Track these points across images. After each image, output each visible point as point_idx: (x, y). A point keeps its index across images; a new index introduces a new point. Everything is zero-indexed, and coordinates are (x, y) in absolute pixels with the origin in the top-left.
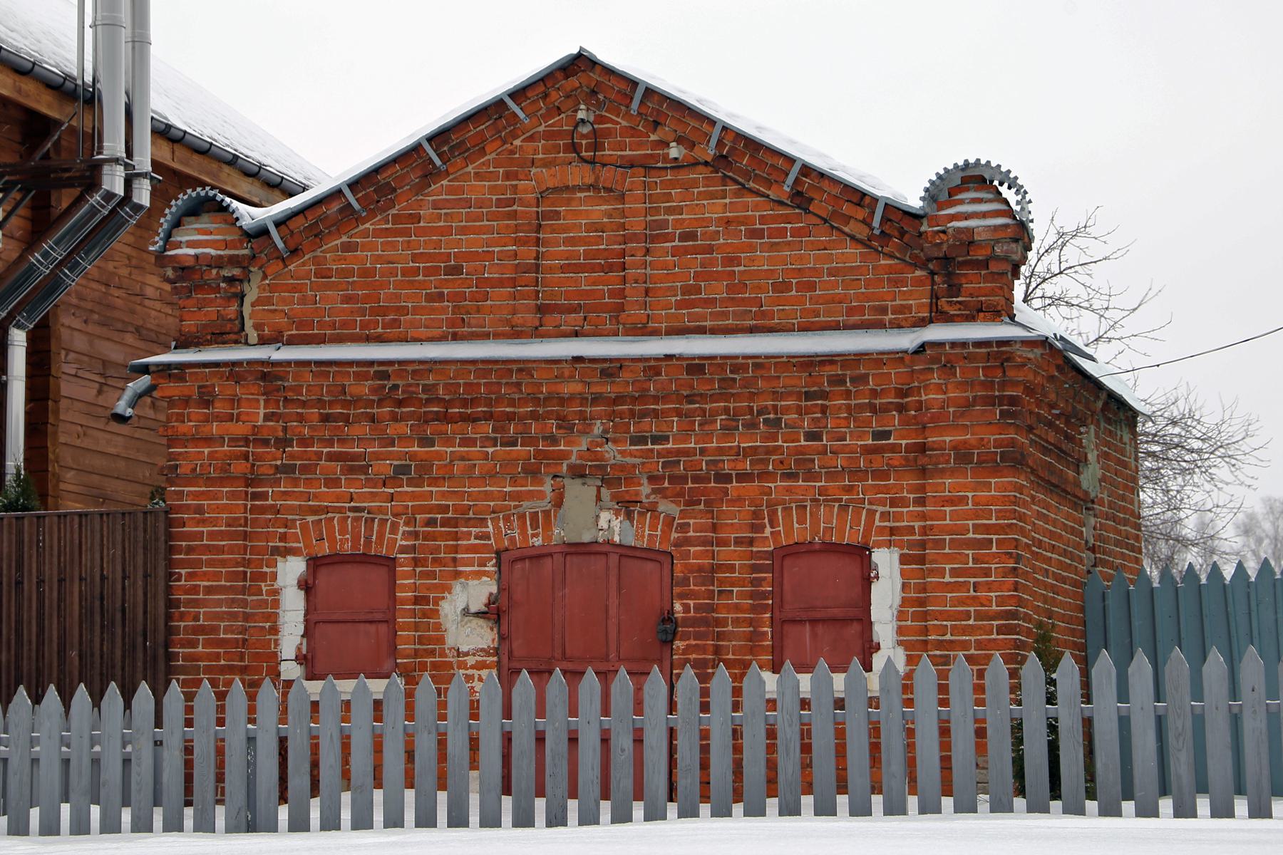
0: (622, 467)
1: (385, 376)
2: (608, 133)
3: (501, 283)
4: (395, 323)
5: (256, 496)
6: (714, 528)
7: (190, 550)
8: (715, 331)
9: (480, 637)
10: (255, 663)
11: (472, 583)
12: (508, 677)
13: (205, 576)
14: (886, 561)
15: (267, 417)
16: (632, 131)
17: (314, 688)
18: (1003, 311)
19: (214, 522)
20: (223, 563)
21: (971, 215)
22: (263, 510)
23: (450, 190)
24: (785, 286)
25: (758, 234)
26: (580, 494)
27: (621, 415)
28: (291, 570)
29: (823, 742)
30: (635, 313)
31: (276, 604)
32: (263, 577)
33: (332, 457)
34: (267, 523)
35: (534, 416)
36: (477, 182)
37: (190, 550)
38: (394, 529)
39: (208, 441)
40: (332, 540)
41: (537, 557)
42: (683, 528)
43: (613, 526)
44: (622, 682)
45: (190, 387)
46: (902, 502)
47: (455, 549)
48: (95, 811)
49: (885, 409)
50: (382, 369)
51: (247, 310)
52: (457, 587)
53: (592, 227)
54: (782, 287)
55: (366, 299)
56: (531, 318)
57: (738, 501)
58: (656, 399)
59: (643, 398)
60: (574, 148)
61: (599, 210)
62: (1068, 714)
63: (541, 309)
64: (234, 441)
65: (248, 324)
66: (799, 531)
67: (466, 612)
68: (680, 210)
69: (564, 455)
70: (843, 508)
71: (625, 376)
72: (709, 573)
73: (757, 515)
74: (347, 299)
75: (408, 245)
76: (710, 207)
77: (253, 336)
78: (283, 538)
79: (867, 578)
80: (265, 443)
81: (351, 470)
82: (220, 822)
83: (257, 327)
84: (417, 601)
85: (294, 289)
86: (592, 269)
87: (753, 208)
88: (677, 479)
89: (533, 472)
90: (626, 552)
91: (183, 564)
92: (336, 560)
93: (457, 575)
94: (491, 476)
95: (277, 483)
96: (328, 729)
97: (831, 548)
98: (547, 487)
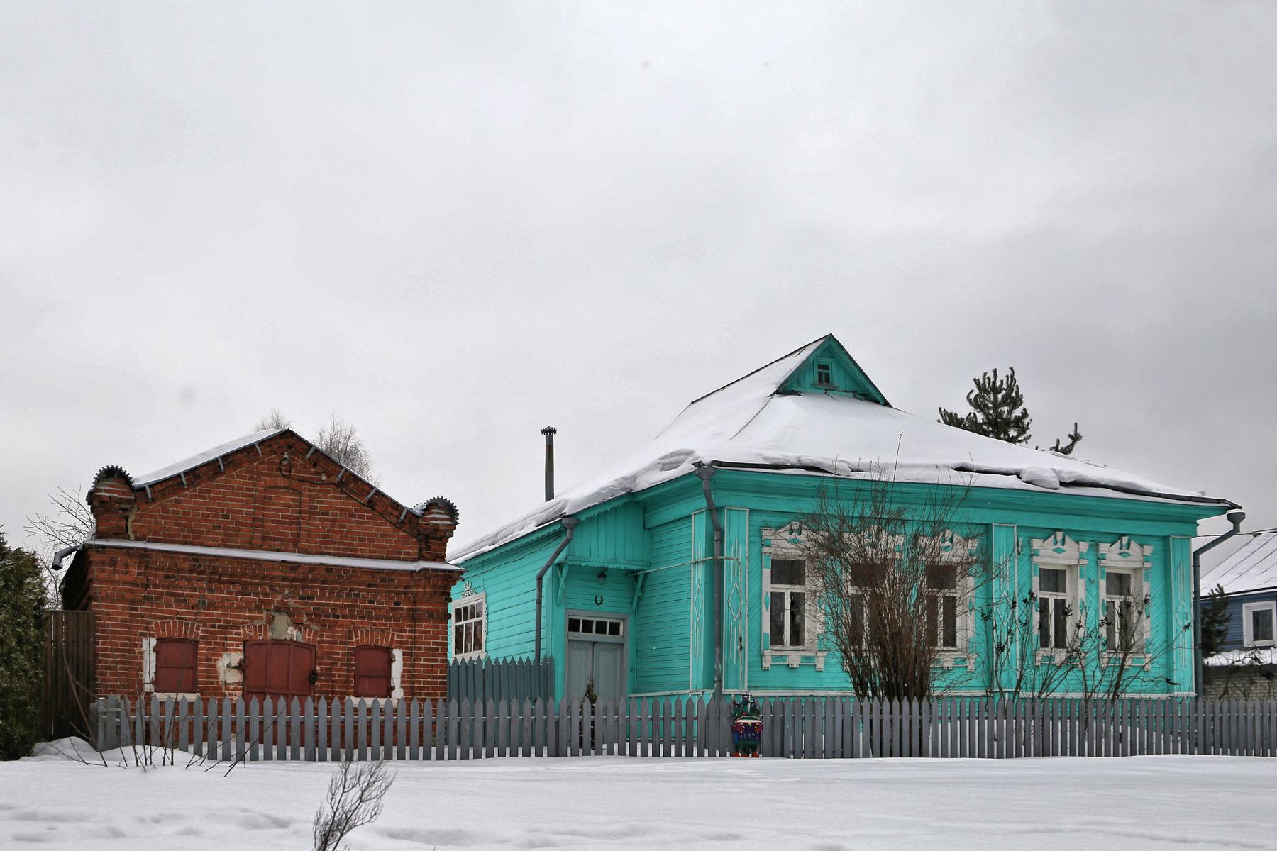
0: (297, 609)
1: (197, 561)
2: (295, 466)
3: (246, 525)
4: (198, 538)
5: (132, 609)
6: (333, 637)
7: (103, 631)
8: (335, 555)
9: (234, 677)
10: (132, 686)
11: (233, 654)
12: (246, 696)
13: (111, 644)
14: (398, 653)
15: (139, 574)
16: (304, 466)
17: (161, 697)
18: (441, 558)
19: (115, 620)
20: (119, 638)
21: (438, 518)
22: (137, 615)
23: (225, 481)
24: (363, 539)
25: (353, 516)
26: (281, 621)
27: (172, 577)
28: (149, 644)
29: (389, 727)
30: (304, 544)
31: (142, 658)
32: (136, 646)
33: (168, 594)
34: (137, 622)
35: (261, 585)
36: (237, 479)
37: (103, 631)
38: (198, 628)
39: (112, 582)
40: (169, 631)
41: (261, 644)
42: (322, 636)
43: (292, 633)
44: (296, 702)
45: (106, 557)
46: (404, 631)
47: (226, 639)
48: (459, 750)
49: (398, 593)
50: (196, 558)
51: (130, 524)
52: (225, 655)
53: (285, 505)
54: (362, 539)
55: (185, 525)
56: (259, 541)
57: (341, 626)
58: (312, 581)
59: (304, 580)
60: (280, 470)
61: (289, 498)
62: (428, 719)
63: (264, 538)
64: (124, 583)
65: (130, 530)
66: (366, 639)
67: (229, 666)
68: (321, 502)
69: (272, 602)
70: (383, 632)
71: (301, 570)
72: (329, 655)
73: (350, 632)
74: (177, 524)
75: (205, 503)
76: (334, 502)
77: (132, 536)
78: (146, 629)
79: (391, 660)
80: (137, 585)
81: (179, 601)
82: (302, 756)
83: (134, 532)
84: (207, 660)
85: (152, 517)
86: (285, 523)
87: (352, 506)
88: (317, 615)
89: (259, 609)
90: (298, 644)
91: (100, 637)
92: (170, 640)
93: (227, 650)
94: (240, 608)
95: (142, 604)
96: (363, 720)
97: (377, 648)
98: (264, 615)
